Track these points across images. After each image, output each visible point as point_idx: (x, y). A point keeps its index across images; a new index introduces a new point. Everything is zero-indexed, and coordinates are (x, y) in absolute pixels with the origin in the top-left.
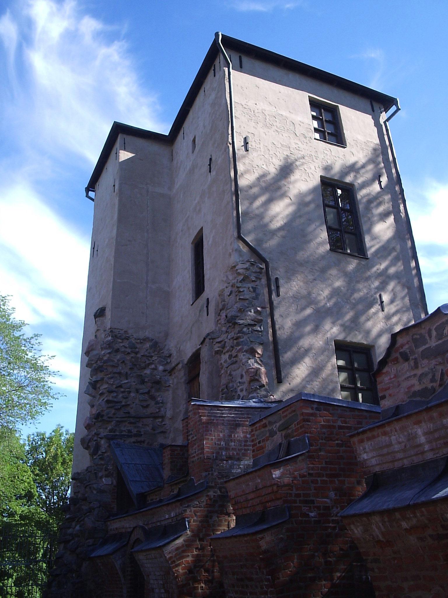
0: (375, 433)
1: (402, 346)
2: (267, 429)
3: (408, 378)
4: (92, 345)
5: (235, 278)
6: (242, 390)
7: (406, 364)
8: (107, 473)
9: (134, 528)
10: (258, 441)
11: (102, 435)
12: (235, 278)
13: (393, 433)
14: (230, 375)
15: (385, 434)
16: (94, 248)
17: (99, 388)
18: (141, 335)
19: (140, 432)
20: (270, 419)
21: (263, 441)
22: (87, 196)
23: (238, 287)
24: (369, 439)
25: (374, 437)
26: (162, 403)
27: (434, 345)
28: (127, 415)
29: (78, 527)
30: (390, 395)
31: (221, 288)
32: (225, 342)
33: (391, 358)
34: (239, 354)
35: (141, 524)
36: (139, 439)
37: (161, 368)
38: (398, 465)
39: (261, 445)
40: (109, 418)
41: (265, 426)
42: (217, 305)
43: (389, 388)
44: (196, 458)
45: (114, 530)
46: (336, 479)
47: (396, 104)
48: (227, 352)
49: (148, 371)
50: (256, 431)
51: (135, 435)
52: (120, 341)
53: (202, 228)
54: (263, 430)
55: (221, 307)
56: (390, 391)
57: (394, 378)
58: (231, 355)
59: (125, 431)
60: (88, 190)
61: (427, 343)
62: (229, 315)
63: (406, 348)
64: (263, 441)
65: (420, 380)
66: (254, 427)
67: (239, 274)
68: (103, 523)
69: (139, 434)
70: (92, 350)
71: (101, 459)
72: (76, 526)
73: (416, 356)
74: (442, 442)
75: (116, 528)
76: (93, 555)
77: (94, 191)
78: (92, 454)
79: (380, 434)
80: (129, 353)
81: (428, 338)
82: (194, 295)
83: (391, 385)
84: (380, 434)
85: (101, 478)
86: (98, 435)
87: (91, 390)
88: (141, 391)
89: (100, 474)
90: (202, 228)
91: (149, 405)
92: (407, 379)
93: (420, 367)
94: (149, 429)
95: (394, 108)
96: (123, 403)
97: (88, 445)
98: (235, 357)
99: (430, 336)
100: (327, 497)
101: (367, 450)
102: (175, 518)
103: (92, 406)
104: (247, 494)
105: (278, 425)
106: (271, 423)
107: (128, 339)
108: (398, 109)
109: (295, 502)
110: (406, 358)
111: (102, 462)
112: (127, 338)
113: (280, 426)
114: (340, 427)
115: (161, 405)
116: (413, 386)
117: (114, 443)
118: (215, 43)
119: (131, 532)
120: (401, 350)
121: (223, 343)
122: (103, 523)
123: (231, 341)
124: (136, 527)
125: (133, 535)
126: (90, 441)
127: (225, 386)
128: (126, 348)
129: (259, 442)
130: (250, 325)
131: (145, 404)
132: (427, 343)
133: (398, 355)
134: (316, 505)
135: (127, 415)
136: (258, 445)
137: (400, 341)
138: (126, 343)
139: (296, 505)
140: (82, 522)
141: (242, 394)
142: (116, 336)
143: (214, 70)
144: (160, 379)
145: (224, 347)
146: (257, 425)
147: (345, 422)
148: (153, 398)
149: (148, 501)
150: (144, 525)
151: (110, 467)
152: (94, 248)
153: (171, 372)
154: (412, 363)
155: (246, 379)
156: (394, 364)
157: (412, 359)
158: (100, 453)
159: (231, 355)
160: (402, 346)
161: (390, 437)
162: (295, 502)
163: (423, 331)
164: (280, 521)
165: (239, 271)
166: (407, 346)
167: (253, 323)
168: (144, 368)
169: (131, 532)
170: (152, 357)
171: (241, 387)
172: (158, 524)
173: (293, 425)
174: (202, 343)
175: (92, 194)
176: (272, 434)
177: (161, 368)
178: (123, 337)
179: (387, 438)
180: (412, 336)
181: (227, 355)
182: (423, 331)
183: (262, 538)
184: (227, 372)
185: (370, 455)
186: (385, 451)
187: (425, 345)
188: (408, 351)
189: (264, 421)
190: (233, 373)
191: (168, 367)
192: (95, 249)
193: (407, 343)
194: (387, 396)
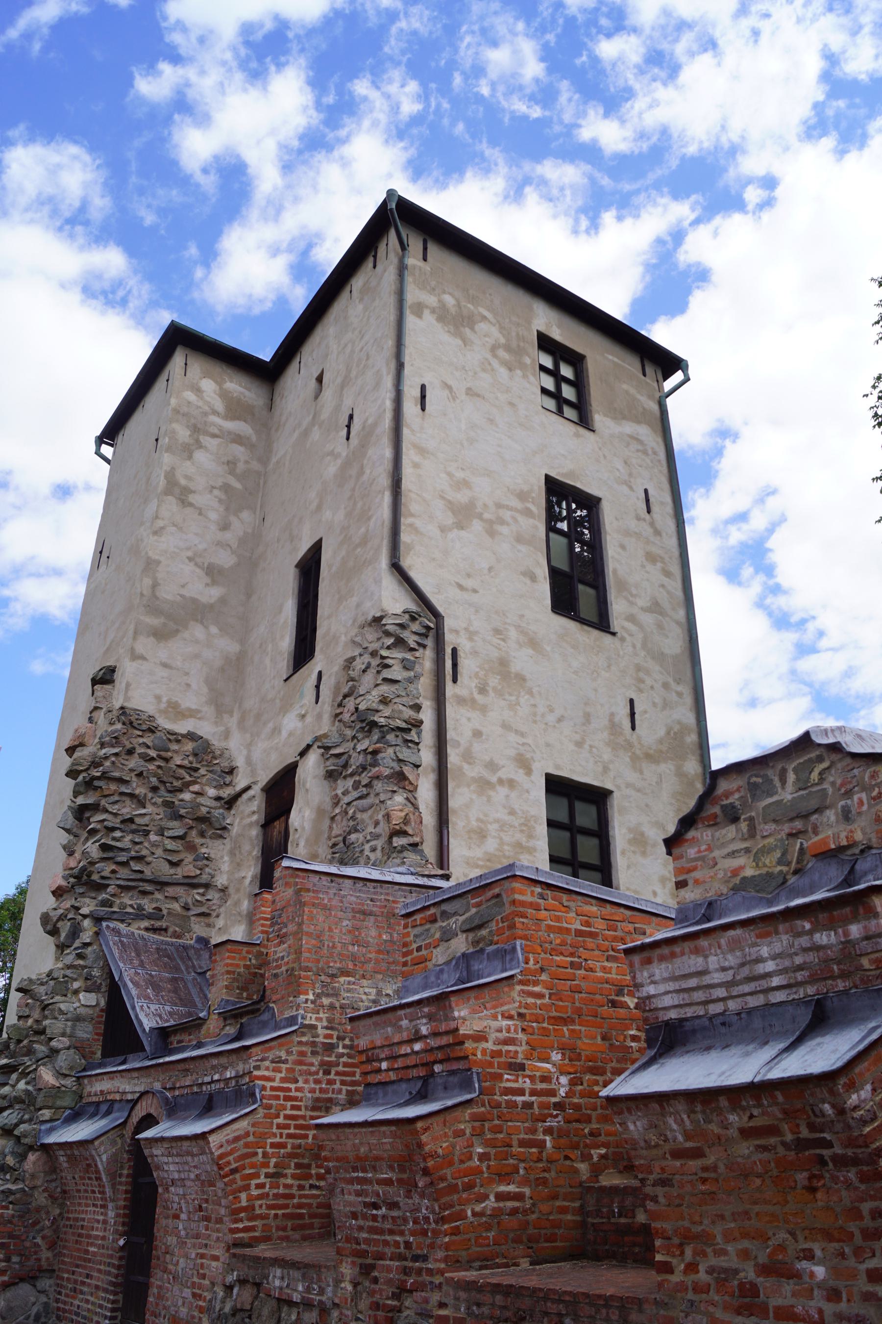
0: (677, 949)
1: (727, 795)
2: (437, 925)
3: (734, 852)
4: (83, 736)
5: (379, 639)
6: (373, 850)
7: (732, 828)
8: (89, 983)
9: (143, 1094)
10: (415, 946)
11: (85, 911)
12: (379, 639)
13: (713, 951)
14: (353, 818)
15: (697, 951)
16: (101, 552)
17: (88, 819)
18: (182, 728)
19: (161, 910)
20: (444, 907)
21: (428, 946)
22: (98, 453)
23: (383, 658)
24: (662, 959)
25: (673, 955)
26: (207, 859)
27: (789, 797)
28: (139, 876)
29: (22, 1085)
30: (697, 882)
31: (349, 654)
32: (350, 757)
33: (704, 814)
34: (375, 782)
35: (157, 1086)
36: (158, 924)
37: (212, 792)
38: (715, 1009)
39: (420, 953)
40: (103, 878)
41: (433, 920)
42: (337, 688)
43: (695, 869)
44: (284, 968)
45: (96, 1095)
46: (565, 1029)
47: (685, 369)
48: (352, 775)
49: (187, 796)
50: (413, 927)
51: (149, 917)
52: (140, 733)
53: (320, 540)
54: (428, 926)
55: (345, 690)
56: (696, 874)
57: (706, 850)
58: (360, 782)
59: (131, 906)
60: (100, 440)
61: (776, 793)
62: (362, 707)
63: (734, 799)
64: (428, 946)
65: (756, 859)
66: (410, 920)
67: (388, 634)
68: (256, 1073)
69: (157, 914)
70: (82, 745)
71: (80, 956)
72: (18, 1081)
73: (753, 814)
74: (806, 973)
75: (102, 1091)
76: (51, 1139)
77: (112, 445)
78: (61, 948)
79: (687, 950)
80: (152, 759)
81: (778, 784)
82: (291, 663)
83: (699, 863)
84: (687, 950)
85: (76, 992)
86: (77, 909)
87: (71, 821)
88: (170, 833)
89: (76, 985)
90: (320, 540)
91: (182, 860)
92: (732, 854)
93: (758, 837)
94: (176, 907)
95: (678, 376)
96: (133, 853)
97: (55, 926)
98: (366, 786)
99: (783, 781)
100: (547, 1060)
101: (657, 978)
102: (233, 1083)
103: (71, 854)
104: (393, 1044)
105: (462, 919)
106: (445, 915)
107: (153, 732)
108: (687, 379)
109: (491, 1065)
110: (734, 818)
111: (81, 962)
112: (151, 730)
113: (464, 922)
114: (579, 933)
115: (205, 862)
116: (742, 868)
117: (108, 927)
118: (383, 207)
119: (135, 1102)
120: (725, 802)
121: (345, 757)
122: (256, 1073)
123: (361, 756)
124: (147, 1092)
125: (138, 1106)
126: (61, 918)
127: (341, 838)
128: (148, 747)
129: (419, 949)
130: (399, 729)
131: (175, 858)
132: (776, 793)
133: (717, 809)
134: (527, 1072)
135: (139, 876)
136: (415, 954)
137: (723, 786)
138: (148, 740)
139: (492, 1071)
140: (32, 1075)
141: (373, 856)
142: (131, 723)
143: (375, 257)
144: (489, 799)
145: (345, 766)
146: (418, 917)
147: (588, 924)
148: (191, 848)
149: (171, 1043)
150: (165, 1088)
151: (96, 973)
152: (101, 552)
153: (230, 803)
154: (744, 826)
155: (383, 829)
156: (709, 826)
157: (745, 820)
158: (77, 943)
159: (360, 782)
160: (727, 795)
161: (706, 957)
162: (491, 1065)
163: (770, 773)
164: (450, 1103)
165: (387, 627)
166: (737, 796)
167: (404, 725)
168: (180, 790)
169: (135, 1102)
170: (196, 770)
171: (373, 843)
172: (195, 1089)
173: (494, 923)
174: (303, 754)
175: (107, 450)
176: (447, 936)
177: (212, 792)
178: (144, 727)
179: (700, 960)
180: (749, 778)
181: (350, 782)
182: (772, 774)
183: (426, 1130)
184: (346, 813)
185: (662, 988)
186: (692, 983)
187: (771, 796)
188: (737, 803)
189: (432, 911)
190: (359, 816)
191: (226, 793)
192: (104, 555)
193: (738, 790)
194: (690, 882)
